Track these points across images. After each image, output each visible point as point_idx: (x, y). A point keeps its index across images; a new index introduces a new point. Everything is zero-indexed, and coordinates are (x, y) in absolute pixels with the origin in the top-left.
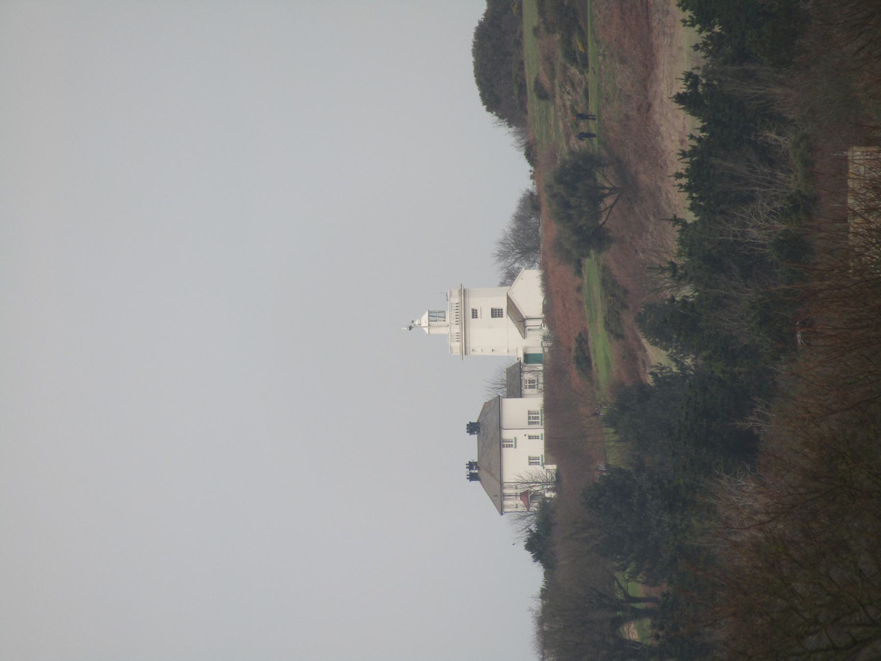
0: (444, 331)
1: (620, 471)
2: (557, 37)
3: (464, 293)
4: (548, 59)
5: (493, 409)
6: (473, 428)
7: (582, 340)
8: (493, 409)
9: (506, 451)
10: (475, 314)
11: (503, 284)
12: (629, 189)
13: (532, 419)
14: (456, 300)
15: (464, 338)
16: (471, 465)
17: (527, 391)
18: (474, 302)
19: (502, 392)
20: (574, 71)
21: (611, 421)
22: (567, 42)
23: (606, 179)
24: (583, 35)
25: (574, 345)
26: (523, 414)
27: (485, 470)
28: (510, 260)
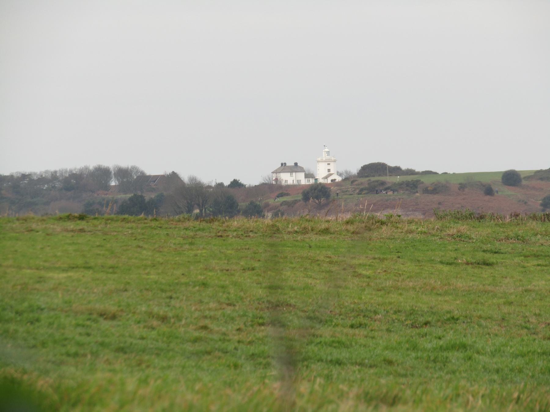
0: (324, 156)
1: (238, 205)
2: (367, 186)
3: (335, 161)
4: (362, 184)
5: (301, 170)
6: (296, 164)
7: (287, 195)
8: (301, 170)
9: (289, 174)
10: (329, 164)
11: (338, 172)
12: (320, 207)
13: (299, 181)
14: (333, 159)
15: (322, 161)
16: (285, 164)
17: (307, 179)
18: (332, 164)
19: (307, 172)
20: (358, 191)
21: (252, 203)
22: (365, 189)
23: (323, 200)
24: (367, 193)
25: (286, 192)
26: (299, 179)
27: (284, 168)
28: (345, 174)
